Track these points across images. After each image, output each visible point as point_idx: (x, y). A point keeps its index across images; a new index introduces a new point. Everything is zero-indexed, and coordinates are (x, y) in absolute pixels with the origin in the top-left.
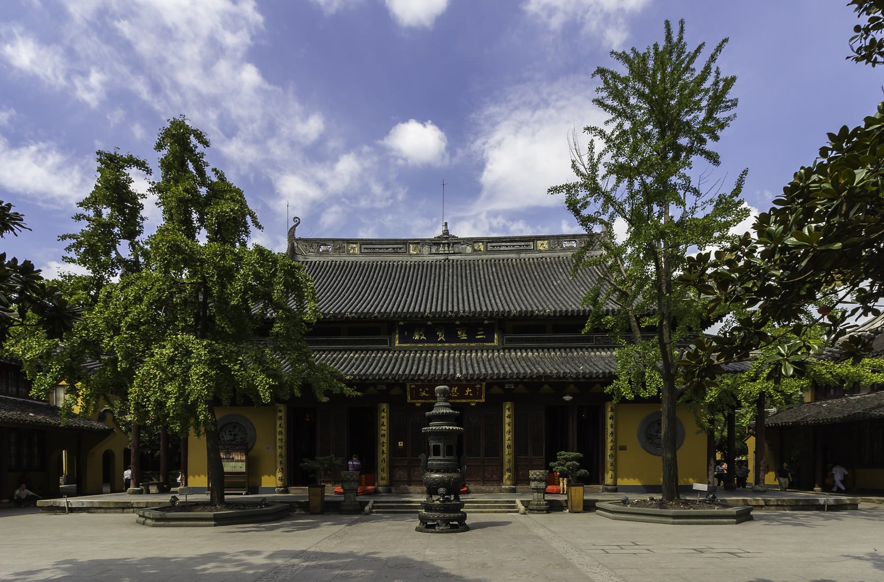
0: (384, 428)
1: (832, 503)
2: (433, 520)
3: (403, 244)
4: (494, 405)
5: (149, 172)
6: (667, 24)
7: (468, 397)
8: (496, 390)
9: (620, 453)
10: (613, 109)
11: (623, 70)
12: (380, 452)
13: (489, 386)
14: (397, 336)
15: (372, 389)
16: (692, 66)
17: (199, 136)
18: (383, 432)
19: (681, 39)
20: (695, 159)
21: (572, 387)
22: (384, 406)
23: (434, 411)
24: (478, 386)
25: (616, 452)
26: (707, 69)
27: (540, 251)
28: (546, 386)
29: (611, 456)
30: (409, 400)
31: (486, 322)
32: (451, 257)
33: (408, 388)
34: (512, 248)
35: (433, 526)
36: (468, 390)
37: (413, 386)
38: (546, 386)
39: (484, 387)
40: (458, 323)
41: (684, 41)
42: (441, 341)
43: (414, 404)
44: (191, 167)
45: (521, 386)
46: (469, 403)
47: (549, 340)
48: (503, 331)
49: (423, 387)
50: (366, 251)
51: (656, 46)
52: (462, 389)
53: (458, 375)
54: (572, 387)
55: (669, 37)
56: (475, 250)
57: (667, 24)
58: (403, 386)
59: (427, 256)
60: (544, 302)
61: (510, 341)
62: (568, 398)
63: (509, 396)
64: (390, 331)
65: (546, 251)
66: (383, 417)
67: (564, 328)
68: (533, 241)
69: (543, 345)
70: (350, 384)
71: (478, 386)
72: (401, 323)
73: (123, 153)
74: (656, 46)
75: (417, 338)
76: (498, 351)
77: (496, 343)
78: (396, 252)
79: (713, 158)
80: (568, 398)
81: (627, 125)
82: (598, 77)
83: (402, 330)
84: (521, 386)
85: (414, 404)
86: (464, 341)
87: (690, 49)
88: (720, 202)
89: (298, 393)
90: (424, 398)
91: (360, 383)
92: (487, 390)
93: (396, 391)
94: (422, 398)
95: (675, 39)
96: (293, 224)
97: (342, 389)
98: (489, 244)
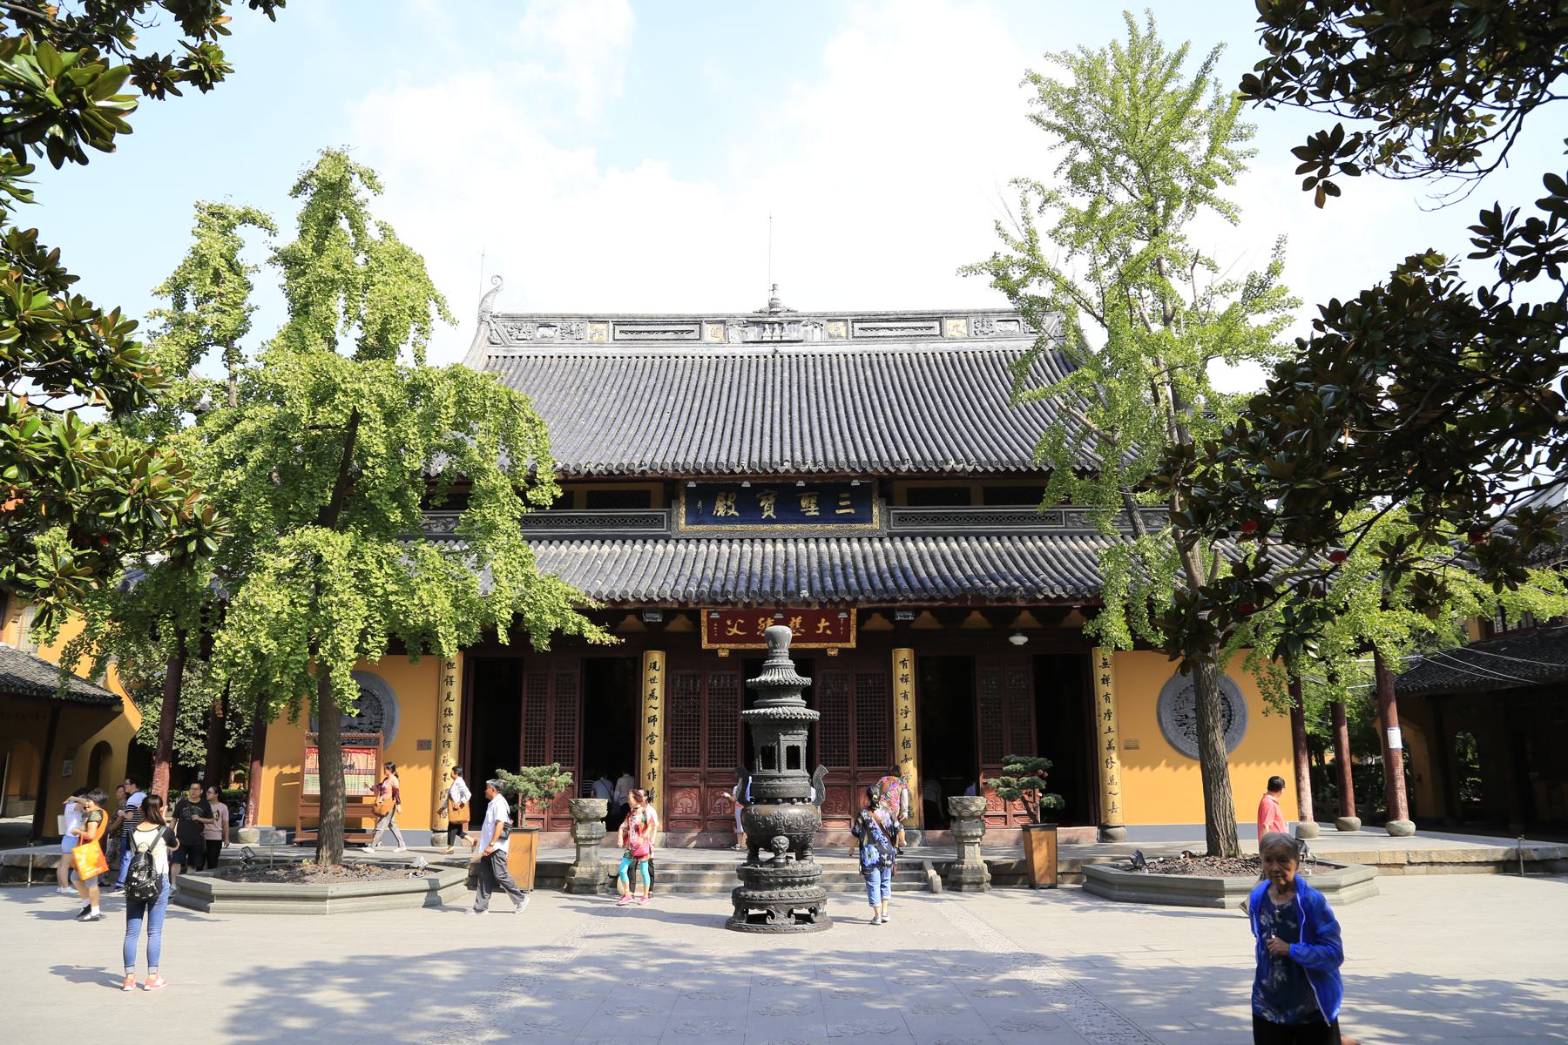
0: (656, 703)
1: (1536, 856)
2: (761, 907)
3: (695, 323)
4: (875, 649)
5: (272, 231)
6: (1127, 15)
7: (823, 638)
8: (877, 622)
9: (429, 735)
10: (1060, 129)
11: (1068, 79)
12: (645, 755)
13: (863, 616)
14: (683, 510)
15: (631, 619)
16: (1178, 71)
17: (370, 179)
18: (652, 712)
19: (1151, 36)
20: (1202, 208)
21: (1025, 615)
22: (657, 657)
23: (763, 678)
24: (843, 615)
25: (437, 736)
26: (1199, 81)
27: (953, 339)
28: (976, 615)
29: (449, 712)
30: (705, 645)
31: (855, 483)
32: (783, 349)
33: (704, 619)
34: (899, 333)
35: (760, 919)
36: (823, 623)
37: (715, 616)
38: (976, 615)
39: (853, 618)
40: (801, 484)
41: (1157, 38)
42: (769, 521)
43: (715, 651)
44: (344, 224)
45: (926, 614)
46: (824, 650)
47: (976, 519)
48: (889, 500)
49: (734, 616)
50: (624, 336)
51: (1114, 45)
52: (810, 622)
53: (805, 593)
54: (1025, 615)
55: (1132, 29)
56: (830, 336)
57: (1127, 15)
58: (694, 615)
59: (736, 345)
60: (963, 451)
61: (902, 519)
62: (1019, 640)
63: (903, 635)
64: (668, 501)
65: (963, 340)
66: (653, 680)
67: (1011, 493)
68: (939, 319)
69: (967, 528)
70: (595, 617)
71: (843, 615)
72: (692, 485)
73: (236, 205)
74: (1114, 45)
75: (721, 512)
76: (881, 540)
77: (876, 524)
78: (680, 337)
79: (1229, 213)
80: (1019, 640)
81: (1084, 156)
82: (1030, 85)
83: (692, 496)
84: (926, 614)
85: (715, 651)
86: (813, 520)
87: (1170, 49)
88: (1249, 287)
89: (503, 638)
90: (735, 639)
91: (611, 613)
92: (860, 623)
93: (679, 624)
94: (735, 639)
95: (1143, 32)
96: (488, 287)
97: (580, 625)
98: (857, 325)
